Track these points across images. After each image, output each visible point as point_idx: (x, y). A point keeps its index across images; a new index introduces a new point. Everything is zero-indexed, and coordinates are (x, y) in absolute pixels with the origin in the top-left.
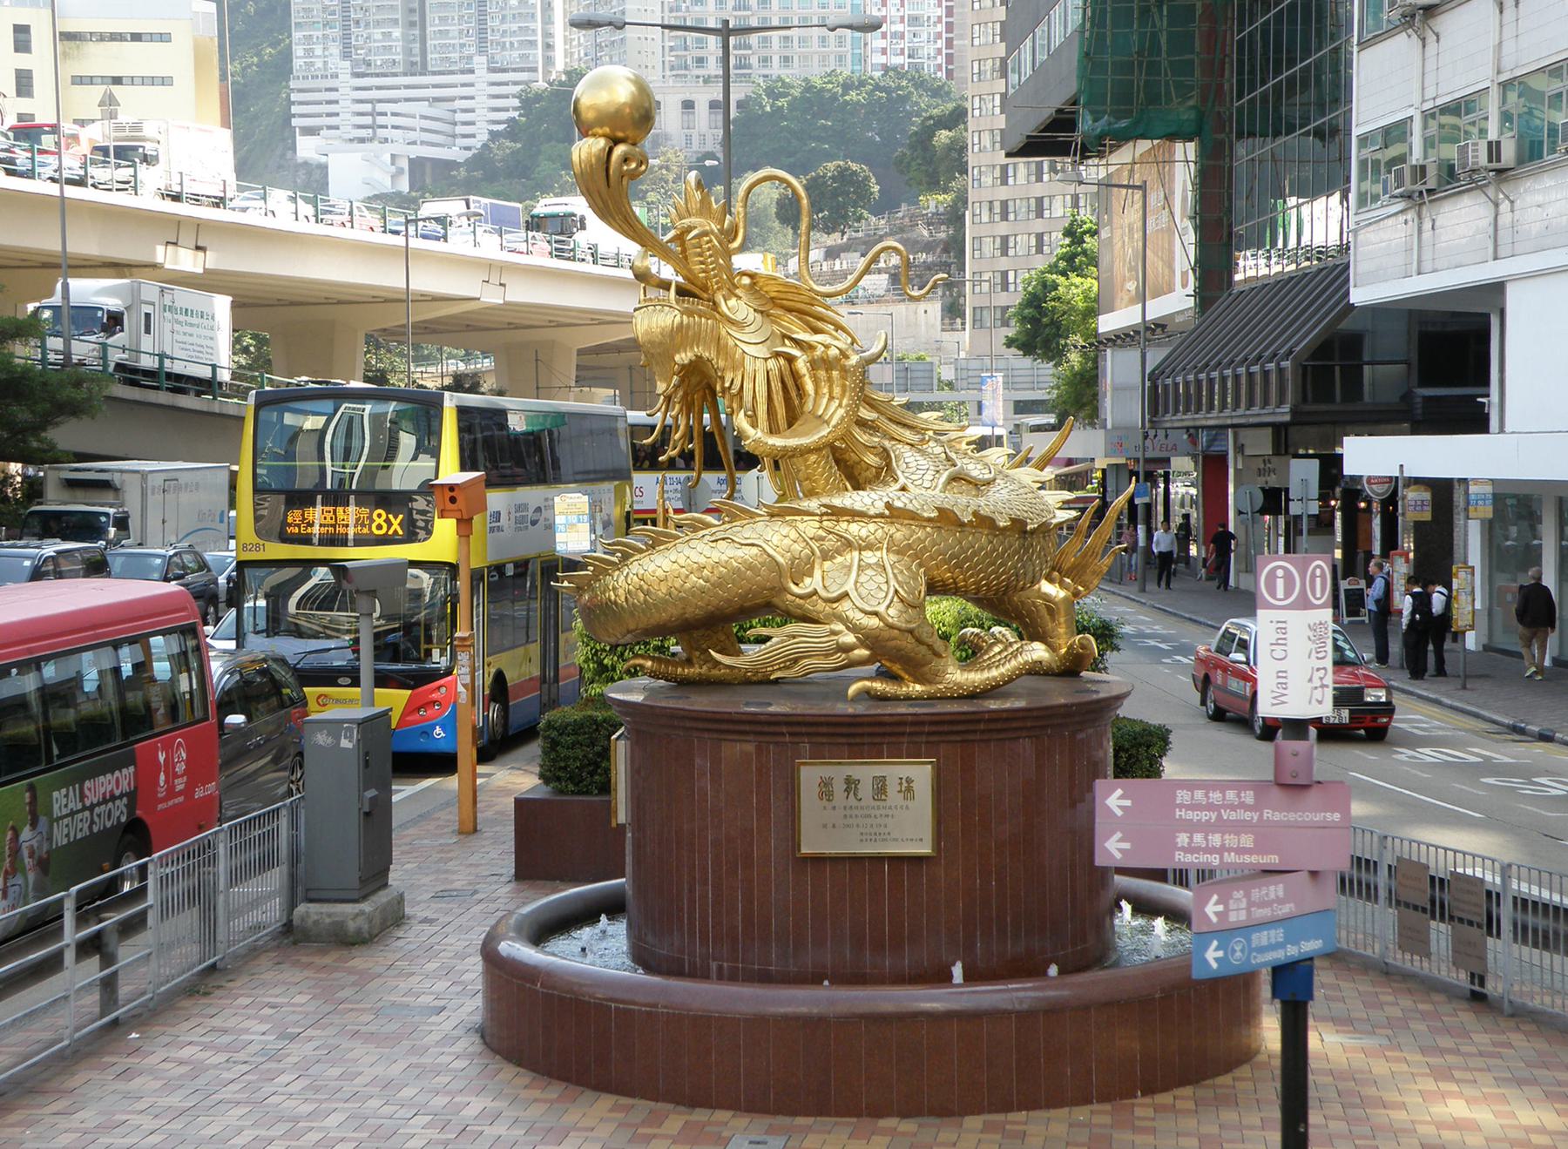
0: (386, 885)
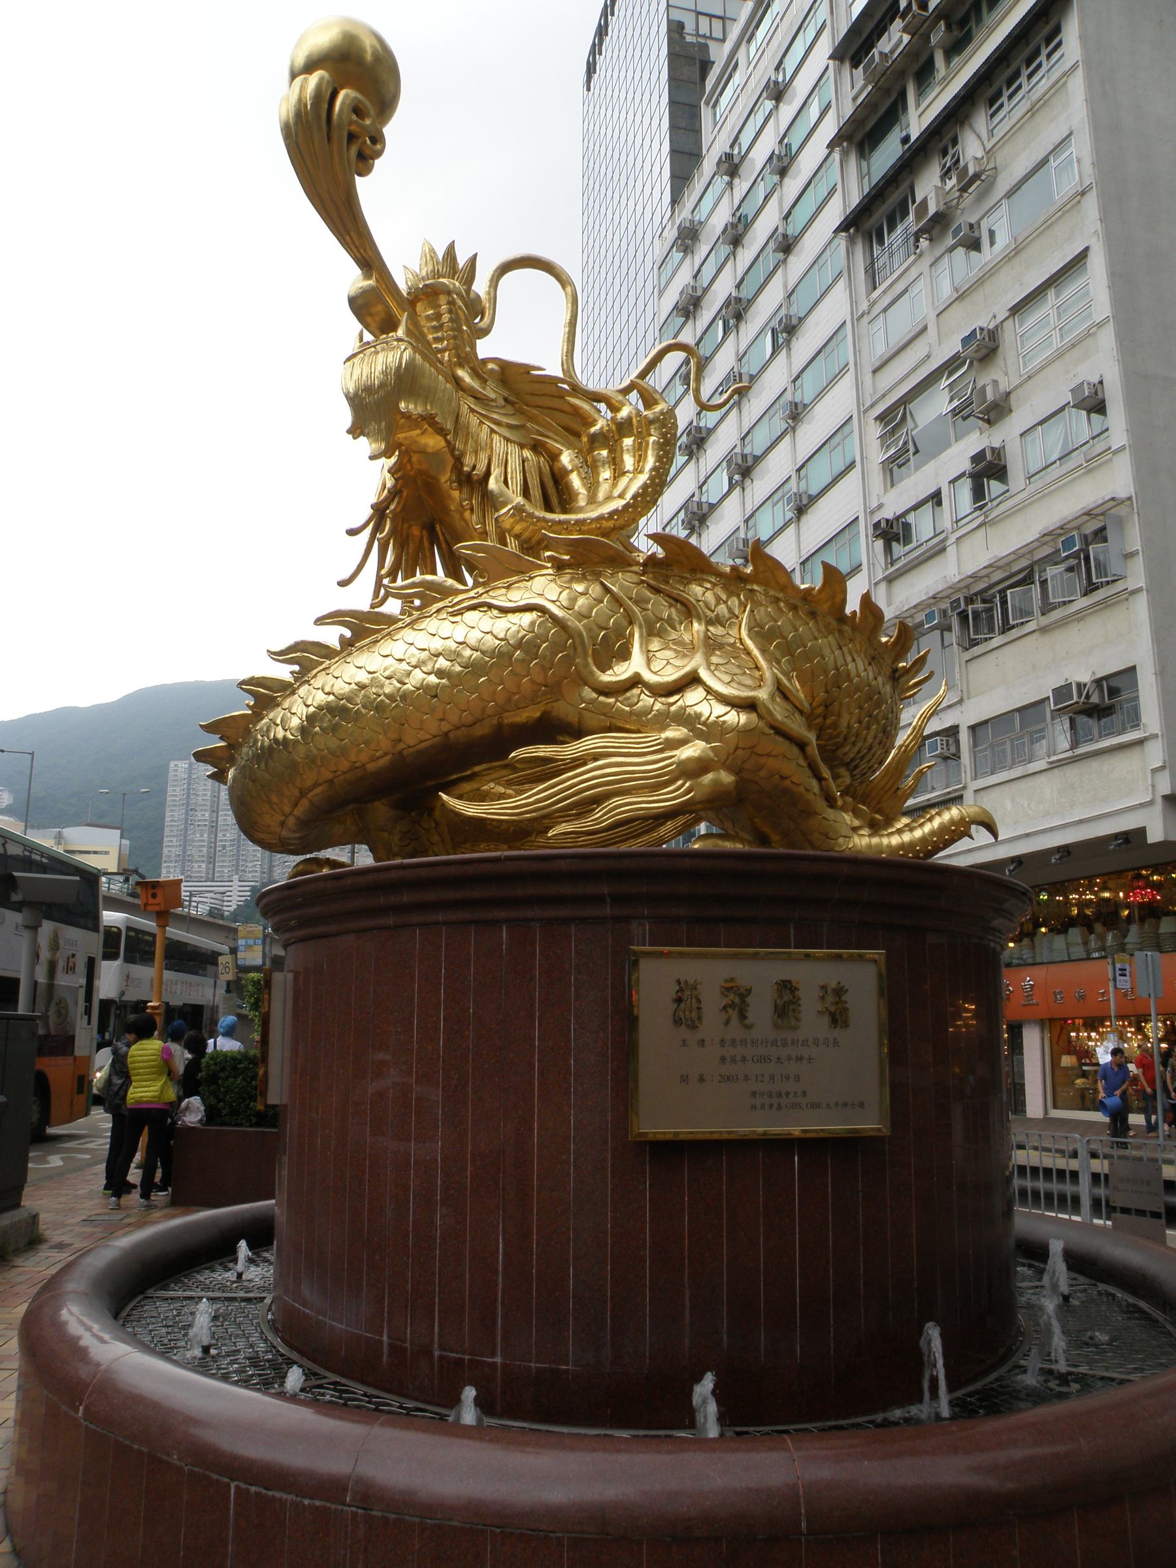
0: (17, 1205)
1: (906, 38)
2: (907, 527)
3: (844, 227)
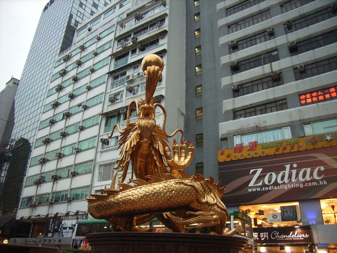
1: (131, 43)
2: (108, 142)
3: (110, 73)
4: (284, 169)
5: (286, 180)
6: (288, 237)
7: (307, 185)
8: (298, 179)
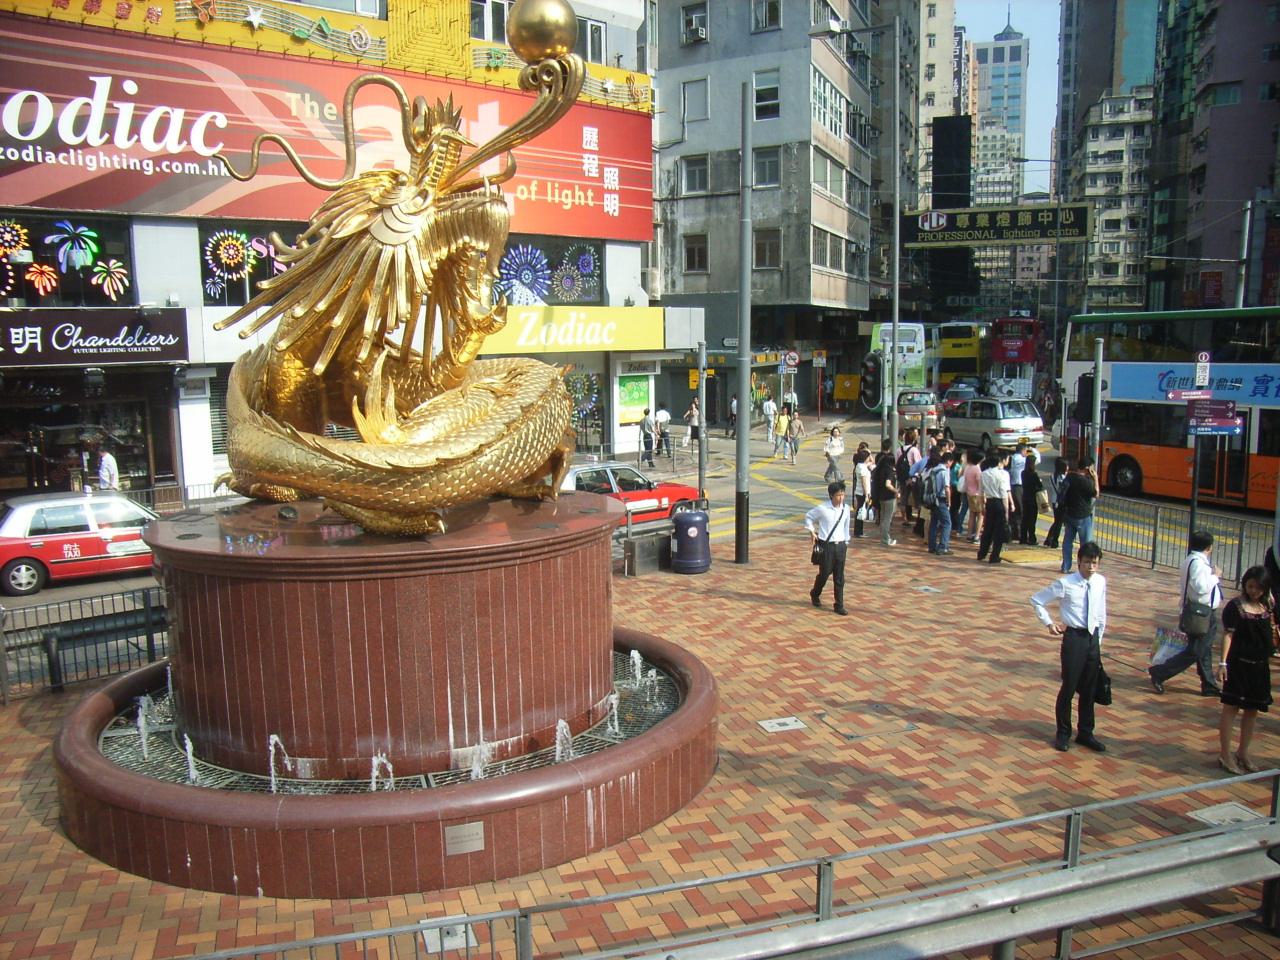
4: (89, 90)
5: (93, 133)
6: (113, 343)
7: (167, 167)
8: (138, 140)
